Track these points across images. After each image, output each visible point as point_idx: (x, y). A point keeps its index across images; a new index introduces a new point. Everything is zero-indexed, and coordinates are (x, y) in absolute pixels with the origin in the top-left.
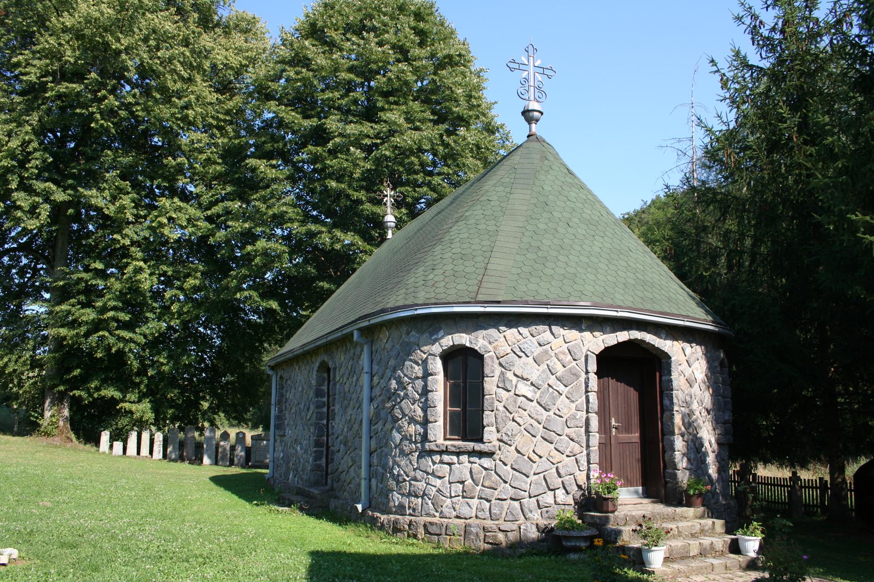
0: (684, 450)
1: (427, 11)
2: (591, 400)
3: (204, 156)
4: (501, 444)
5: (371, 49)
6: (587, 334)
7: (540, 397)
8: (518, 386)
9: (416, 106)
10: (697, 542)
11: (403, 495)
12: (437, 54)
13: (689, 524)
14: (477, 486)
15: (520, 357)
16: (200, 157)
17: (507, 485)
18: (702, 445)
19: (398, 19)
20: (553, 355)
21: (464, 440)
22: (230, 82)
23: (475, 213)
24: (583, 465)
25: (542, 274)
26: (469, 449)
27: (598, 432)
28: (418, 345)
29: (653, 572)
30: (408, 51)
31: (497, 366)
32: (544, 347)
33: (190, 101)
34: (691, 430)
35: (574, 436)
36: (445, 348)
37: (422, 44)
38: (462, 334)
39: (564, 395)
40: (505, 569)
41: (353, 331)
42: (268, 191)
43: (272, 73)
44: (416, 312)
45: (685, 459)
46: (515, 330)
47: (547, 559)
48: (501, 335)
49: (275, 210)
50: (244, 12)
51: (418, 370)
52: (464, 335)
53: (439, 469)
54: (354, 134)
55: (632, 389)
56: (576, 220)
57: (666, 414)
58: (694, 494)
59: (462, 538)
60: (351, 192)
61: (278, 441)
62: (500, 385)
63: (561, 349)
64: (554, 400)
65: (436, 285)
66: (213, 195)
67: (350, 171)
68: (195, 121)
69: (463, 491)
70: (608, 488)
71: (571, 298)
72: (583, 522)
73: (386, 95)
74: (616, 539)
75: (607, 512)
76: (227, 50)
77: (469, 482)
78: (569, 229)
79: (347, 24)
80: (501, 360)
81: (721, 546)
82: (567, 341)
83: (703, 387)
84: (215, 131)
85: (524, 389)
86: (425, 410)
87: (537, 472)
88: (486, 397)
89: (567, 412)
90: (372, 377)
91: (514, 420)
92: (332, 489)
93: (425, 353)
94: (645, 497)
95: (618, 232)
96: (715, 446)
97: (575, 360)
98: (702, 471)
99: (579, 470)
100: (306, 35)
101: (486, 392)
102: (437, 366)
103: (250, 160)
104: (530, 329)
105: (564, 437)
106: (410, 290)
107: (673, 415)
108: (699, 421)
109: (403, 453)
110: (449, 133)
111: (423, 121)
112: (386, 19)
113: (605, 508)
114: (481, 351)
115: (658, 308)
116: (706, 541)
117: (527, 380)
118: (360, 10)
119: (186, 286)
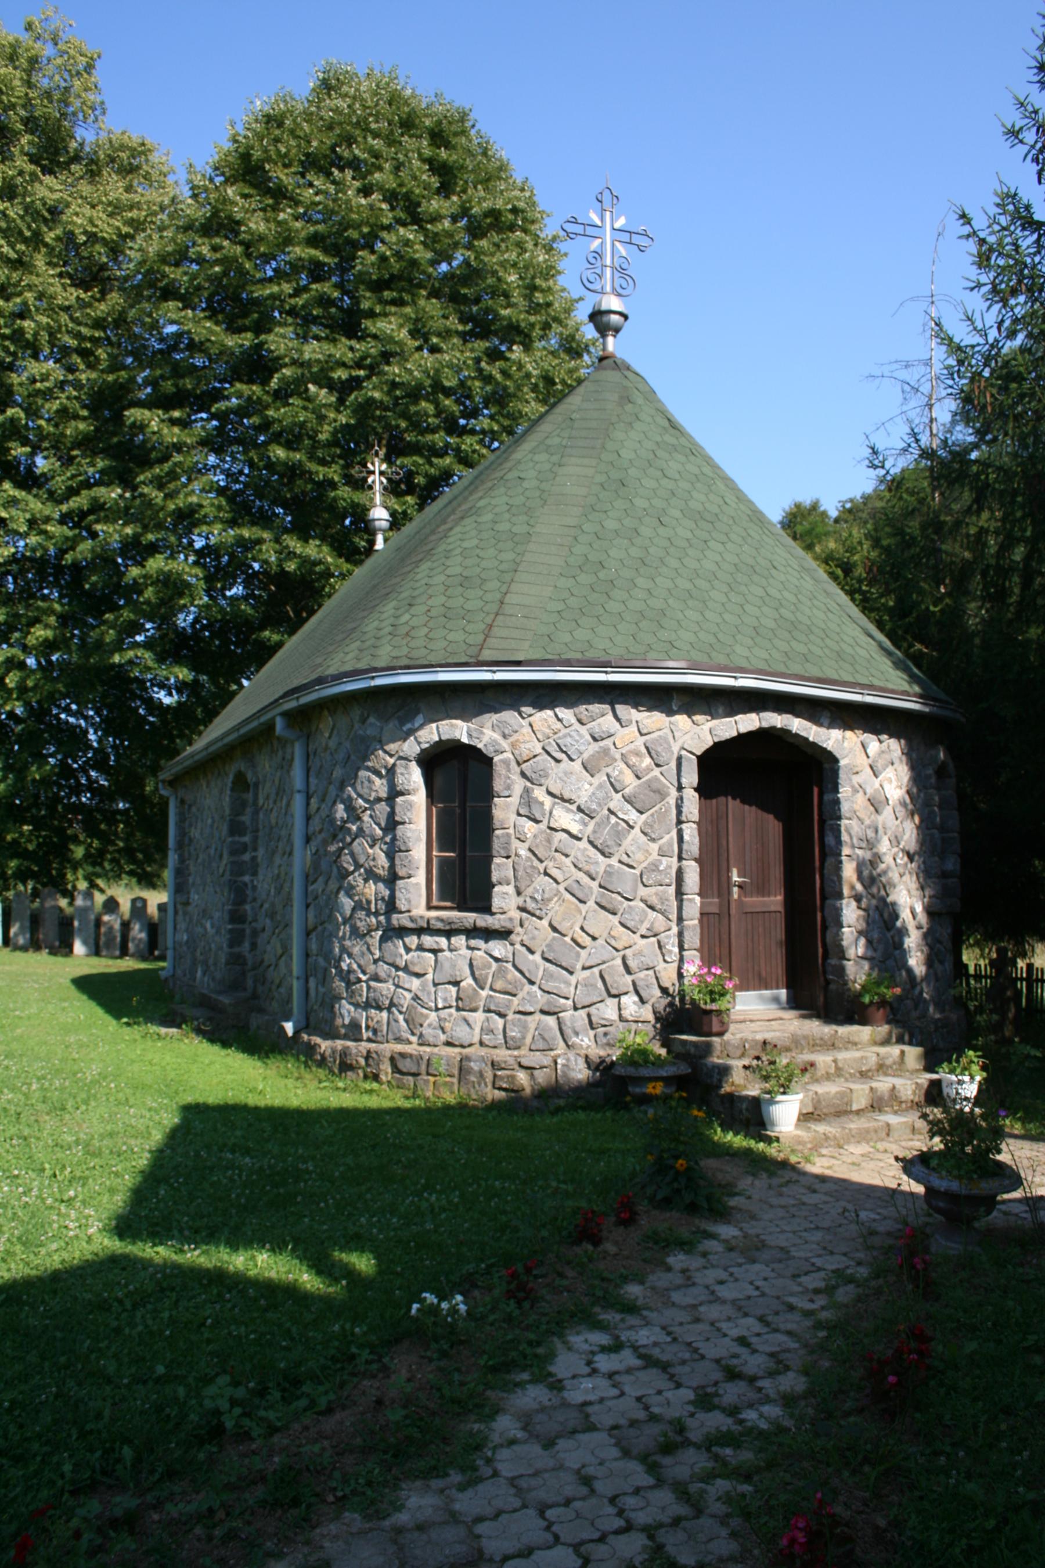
0: (862, 925)
1: (454, 128)
2: (686, 837)
3: (55, 405)
4: (525, 915)
5: (348, 201)
6: (681, 720)
7: (594, 832)
8: (554, 812)
9: (432, 307)
10: (866, 1087)
11: (356, 1005)
12: (471, 208)
13: (858, 1054)
14: (483, 989)
15: (558, 761)
16: (47, 406)
17: (535, 988)
18: (897, 917)
19: (400, 143)
20: (618, 756)
21: (460, 908)
22: (103, 267)
23: (494, 502)
24: (670, 952)
25: (602, 611)
26: (467, 925)
27: (699, 894)
28: (380, 741)
29: (778, 1140)
30: (419, 205)
31: (516, 777)
32: (602, 744)
33: (25, 303)
34: (874, 890)
35: (654, 900)
36: (425, 746)
37: (445, 190)
38: (454, 721)
39: (637, 830)
40: (519, 1135)
41: (273, 719)
42: (167, 466)
43: (169, 249)
44: (373, 683)
45: (862, 941)
46: (549, 712)
47: (599, 1116)
48: (524, 723)
49: (180, 502)
50: (123, 133)
51: (380, 786)
52: (458, 722)
53: (416, 960)
54: (318, 361)
55: (771, 817)
56: (677, 514)
57: (830, 861)
58: (871, 1002)
59: (455, 1080)
60: (312, 466)
61: (180, 913)
62: (522, 812)
63: (632, 746)
64: (618, 837)
65: (412, 633)
66: (73, 477)
67: (312, 429)
68: (36, 339)
69: (458, 999)
70: (711, 992)
71: (652, 655)
72: (669, 1052)
73: (378, 286)
74: (720, 1081)
75: (710, 1034)
76: (93, 207)
77: (468, 982)
78: (661, 530)
79: (307, 155)
80: (524, 766)
81: (910, 1092)
82: (644, 731)
83: (901, 812)
84: (76, 359)
85: (566, 818)
86: (391, 856)
87: (587, 964)
88: (497, 832)
89: (642, 858)
90: (308, 798)
91: (546, 874)
92: (255, 996)
93: (391, 756)
94: (792, 1008)
95: (752, 533)
96: (922, 918)
97: (658, 765)
98: (896, 961)
99: (665, 961)
100: (233, 176)
101: (496, 823)
102: (414, 777)
103: (132, 411)
104: (577, 710)
105: (638, 904)
106: (368, 643)
107: (841, 862)
108: (890, 874)
109: (355, 933)
110: (494, 355)
111: (446, 334)
112: (376, 143)
113: (705, 1029)
114: (489, 752)
115: (815, 672)
116: (883, 1084)
117: (570, 801)
118: (330, 128)
119: (31, 641)
